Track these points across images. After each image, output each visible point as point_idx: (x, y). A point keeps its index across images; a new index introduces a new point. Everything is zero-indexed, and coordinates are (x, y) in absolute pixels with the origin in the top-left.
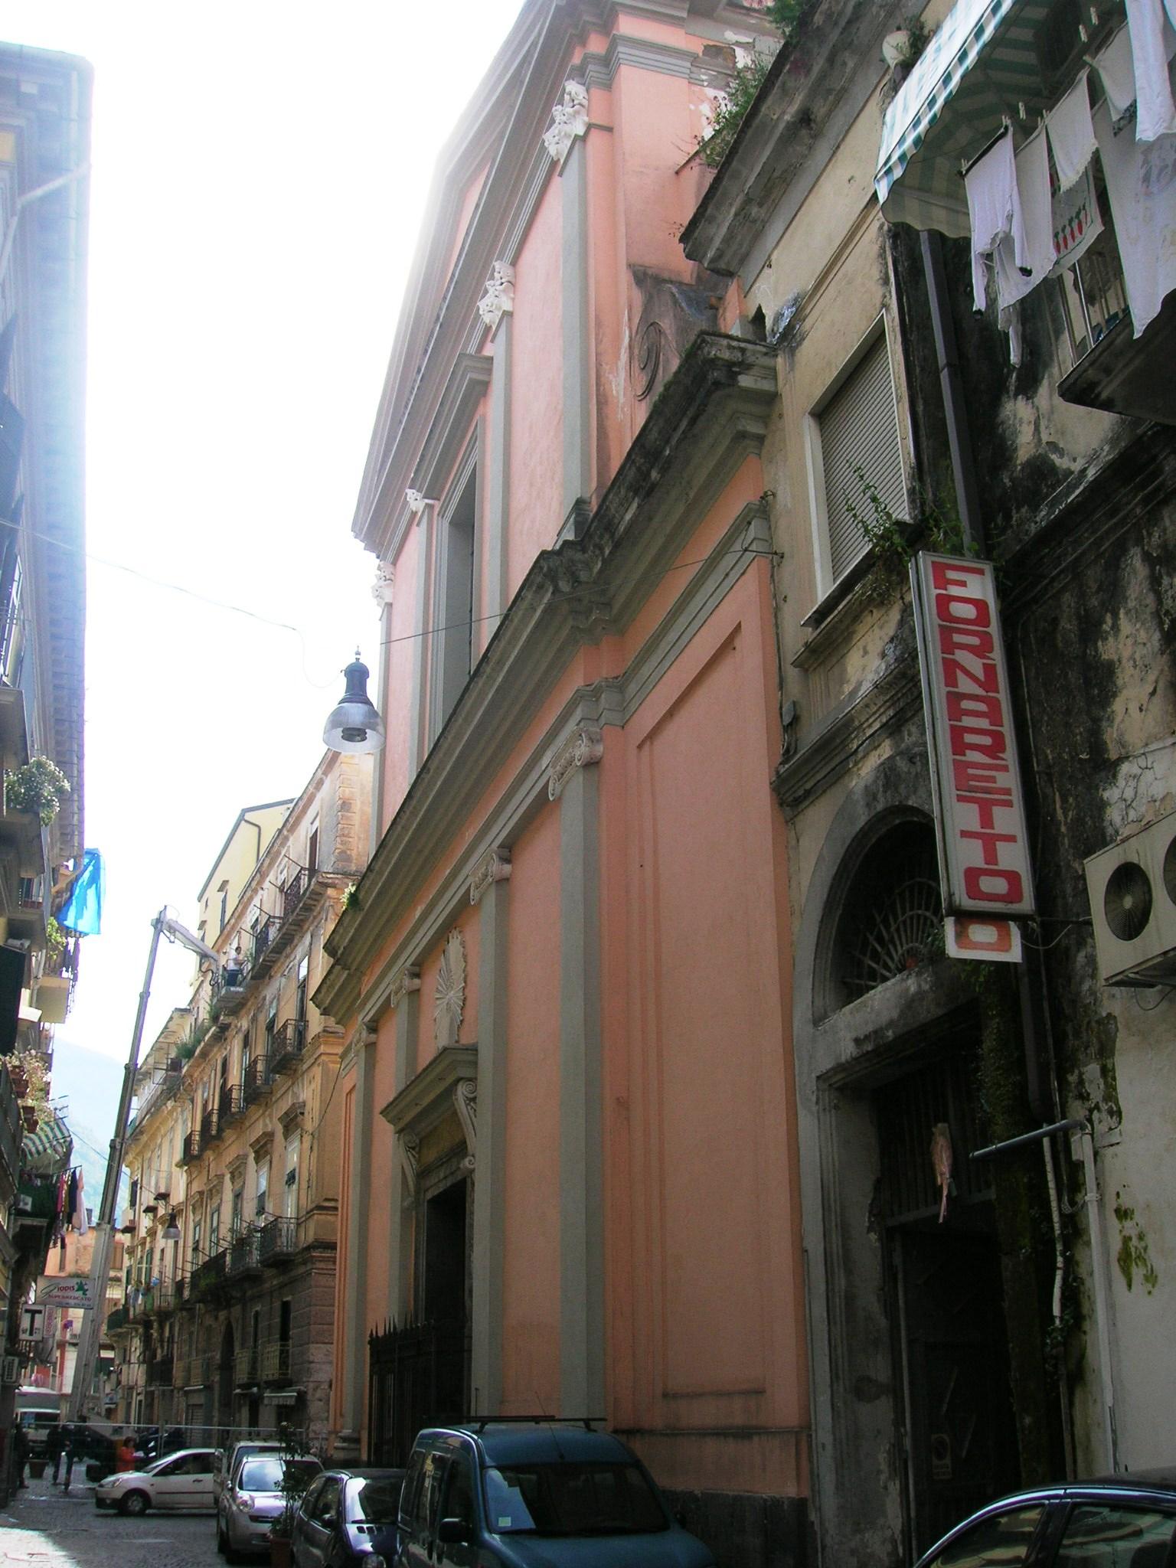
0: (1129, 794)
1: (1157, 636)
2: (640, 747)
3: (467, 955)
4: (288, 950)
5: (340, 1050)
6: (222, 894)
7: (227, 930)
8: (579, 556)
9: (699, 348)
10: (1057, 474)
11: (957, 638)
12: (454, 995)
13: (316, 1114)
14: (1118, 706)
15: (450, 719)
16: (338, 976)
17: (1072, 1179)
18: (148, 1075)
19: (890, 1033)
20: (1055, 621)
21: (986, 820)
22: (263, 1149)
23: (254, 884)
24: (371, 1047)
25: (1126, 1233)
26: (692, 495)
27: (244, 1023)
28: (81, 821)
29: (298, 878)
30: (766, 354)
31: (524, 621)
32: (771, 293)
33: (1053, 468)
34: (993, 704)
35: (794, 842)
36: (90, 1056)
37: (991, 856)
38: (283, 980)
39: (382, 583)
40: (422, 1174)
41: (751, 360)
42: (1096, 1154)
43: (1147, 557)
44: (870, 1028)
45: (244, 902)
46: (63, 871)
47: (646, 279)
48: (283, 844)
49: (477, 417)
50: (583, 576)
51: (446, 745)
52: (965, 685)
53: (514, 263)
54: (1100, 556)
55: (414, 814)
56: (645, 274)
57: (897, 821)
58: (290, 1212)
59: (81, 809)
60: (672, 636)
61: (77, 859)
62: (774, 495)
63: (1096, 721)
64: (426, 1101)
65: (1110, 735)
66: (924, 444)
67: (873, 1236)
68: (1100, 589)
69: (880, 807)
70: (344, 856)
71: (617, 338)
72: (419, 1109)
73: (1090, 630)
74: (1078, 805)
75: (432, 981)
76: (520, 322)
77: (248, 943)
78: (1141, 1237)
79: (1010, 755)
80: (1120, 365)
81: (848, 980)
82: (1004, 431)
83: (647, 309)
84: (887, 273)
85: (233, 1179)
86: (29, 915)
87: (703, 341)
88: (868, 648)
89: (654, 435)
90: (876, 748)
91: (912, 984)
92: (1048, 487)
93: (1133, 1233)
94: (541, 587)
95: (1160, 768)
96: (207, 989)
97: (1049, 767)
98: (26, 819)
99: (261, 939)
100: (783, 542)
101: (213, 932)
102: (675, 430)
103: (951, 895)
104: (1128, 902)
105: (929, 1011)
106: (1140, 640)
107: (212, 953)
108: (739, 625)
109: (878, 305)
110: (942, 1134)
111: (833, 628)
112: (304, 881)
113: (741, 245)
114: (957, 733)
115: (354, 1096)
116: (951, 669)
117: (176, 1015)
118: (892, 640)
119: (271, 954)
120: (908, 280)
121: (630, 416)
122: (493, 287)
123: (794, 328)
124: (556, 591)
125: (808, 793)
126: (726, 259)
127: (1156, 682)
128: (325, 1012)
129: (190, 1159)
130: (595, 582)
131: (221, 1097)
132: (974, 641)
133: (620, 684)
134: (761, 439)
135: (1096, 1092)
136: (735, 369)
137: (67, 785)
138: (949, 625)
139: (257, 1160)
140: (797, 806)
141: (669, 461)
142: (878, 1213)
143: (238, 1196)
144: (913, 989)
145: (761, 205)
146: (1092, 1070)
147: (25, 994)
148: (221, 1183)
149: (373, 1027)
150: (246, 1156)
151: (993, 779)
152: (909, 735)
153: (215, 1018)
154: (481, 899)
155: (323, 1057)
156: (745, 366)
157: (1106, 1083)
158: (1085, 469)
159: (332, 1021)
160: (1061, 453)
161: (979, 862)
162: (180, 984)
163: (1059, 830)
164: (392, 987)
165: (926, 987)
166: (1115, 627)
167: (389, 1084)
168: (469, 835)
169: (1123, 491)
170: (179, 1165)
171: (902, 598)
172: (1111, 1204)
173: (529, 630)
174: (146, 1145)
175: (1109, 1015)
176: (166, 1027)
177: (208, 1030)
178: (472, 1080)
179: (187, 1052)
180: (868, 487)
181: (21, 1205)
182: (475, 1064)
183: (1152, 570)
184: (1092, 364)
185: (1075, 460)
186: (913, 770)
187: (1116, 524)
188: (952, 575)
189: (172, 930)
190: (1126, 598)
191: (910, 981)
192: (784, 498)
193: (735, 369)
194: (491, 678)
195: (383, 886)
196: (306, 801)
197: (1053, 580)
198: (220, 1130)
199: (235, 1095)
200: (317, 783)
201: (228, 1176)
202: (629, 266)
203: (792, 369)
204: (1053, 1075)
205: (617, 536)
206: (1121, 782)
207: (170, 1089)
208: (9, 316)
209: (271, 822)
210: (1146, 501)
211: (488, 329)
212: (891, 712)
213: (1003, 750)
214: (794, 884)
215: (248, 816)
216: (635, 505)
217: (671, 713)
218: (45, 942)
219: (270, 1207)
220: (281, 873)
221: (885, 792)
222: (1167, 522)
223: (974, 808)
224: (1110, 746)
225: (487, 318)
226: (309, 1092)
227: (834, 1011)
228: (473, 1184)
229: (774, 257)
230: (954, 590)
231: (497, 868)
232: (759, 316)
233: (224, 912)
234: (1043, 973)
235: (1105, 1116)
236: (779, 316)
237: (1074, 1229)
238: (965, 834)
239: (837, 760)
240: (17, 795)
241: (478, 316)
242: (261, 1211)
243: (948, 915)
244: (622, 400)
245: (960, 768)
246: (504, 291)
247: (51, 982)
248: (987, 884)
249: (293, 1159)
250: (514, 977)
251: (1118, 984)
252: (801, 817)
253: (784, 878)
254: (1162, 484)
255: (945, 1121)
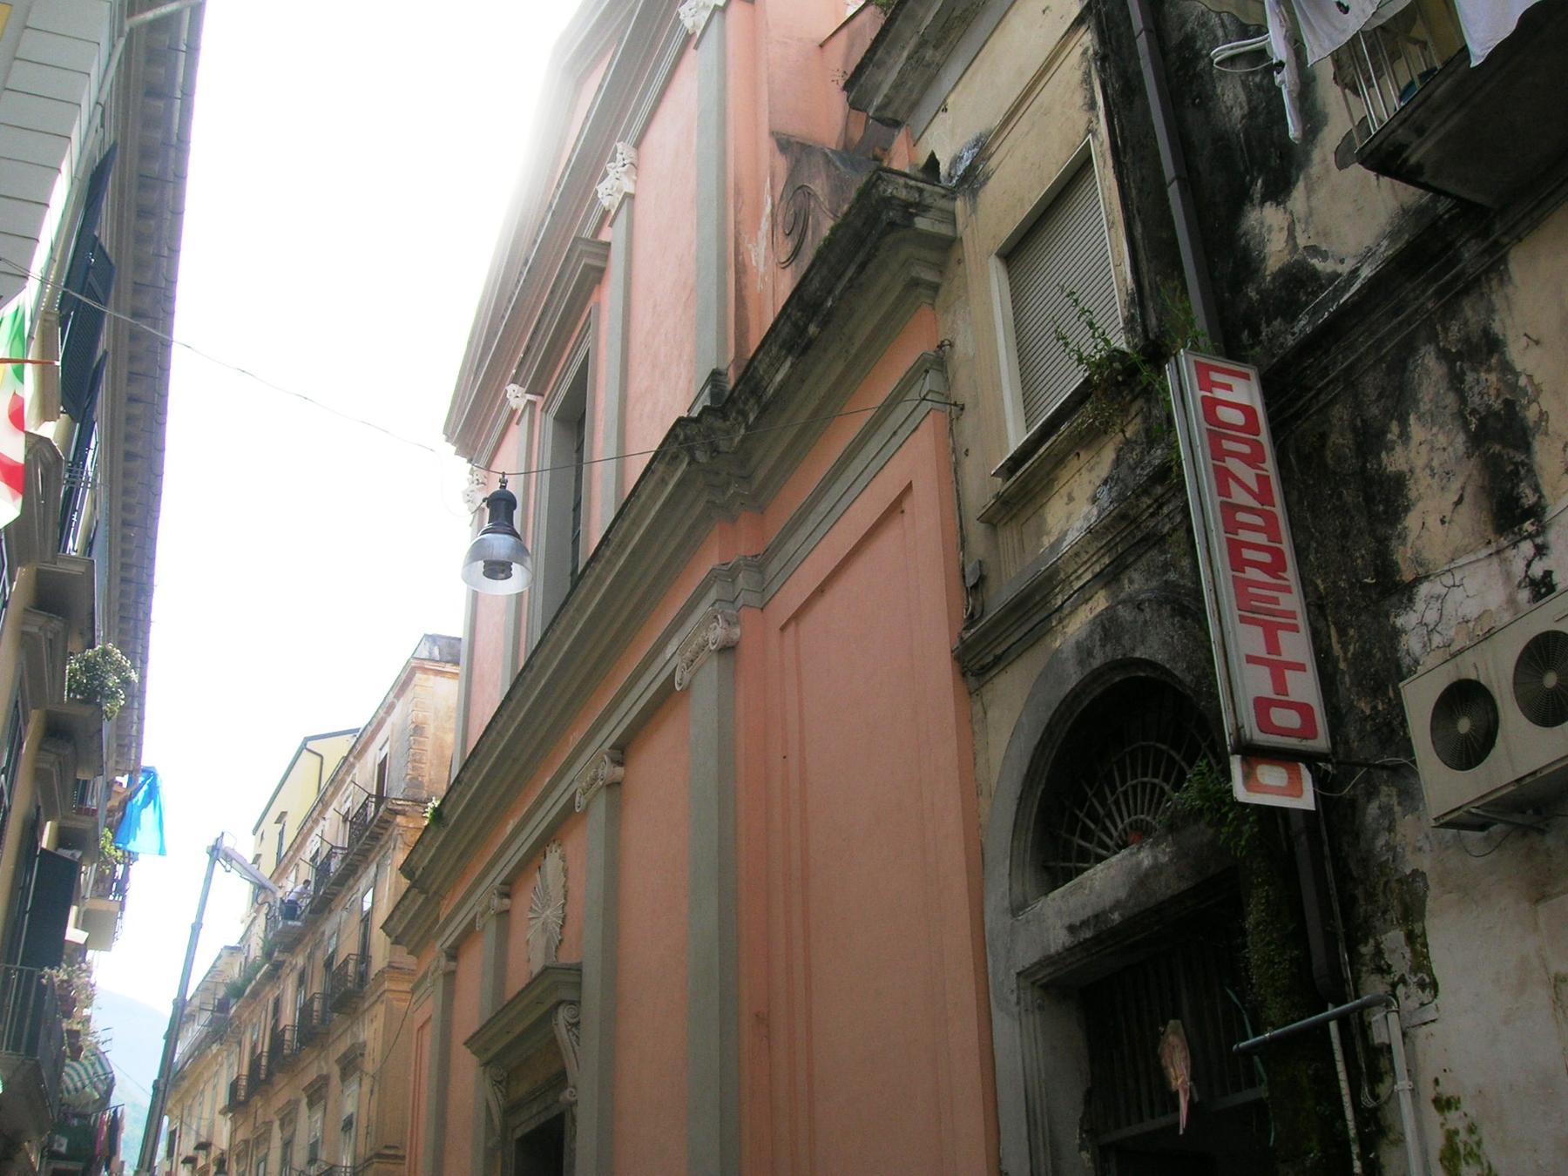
0: (1431, 617)
1: (1461, 438)
2: (783, 629)
3: (568, 871)
4: (351, 882)
5: (407, 987)
6: (280, 827)
7: (283, 864)
8: (718, 424)
9: (874, 185)
10: (1319, 279)
11: (1228, 445)
12: (551, 914)
13: (378, 1056)
14: (1412, 521)
15: (551, 624)
16: (414, 901)
17: (1372, 1064)
18: (192, 1017)
19: (1116, 916)
20: (1323, 436)
21: (1273, 645)
22: (317, 1093)
23: (315, 815)
24: (450, 976)
25: (1450, 1126)
26: (853, 351)
27: (300, 961)
28: (140, 731)
29: (365, 806)
30: (944, 196)
31: (653, 498)
32: (945, 138)
33: (1314, 274)
34: (1270, 518)
35: (981, 714)
36: (148, 969)
37: (1280, 685)
38: (345, 914)
39: (475, 487)
40: (511, 1110)
41: (929, 201)
42: (1404, 1035)
43: (1443, 354)
44: (1089, 912)
45: (304, 833)
46: (116, 788)
47: (791, 147)
48: (348, 772)
49: (591, 304)
50: (723, 445)
51: (553, 639)
52: (1240, 497)
53: (637, 145)
54: (1380, 360)
55: (512, 718)
56: (789, 142)
57: (1117, 679)
58: (346, 1161)
59: (141, 719)
60: (824, 507)
61: (133, 774)
62: (951, 345)
63: (1383, 541)
64: (518, 1029)
65: (1402, 556)
66: (1144, 266)
67: (1085, 1155)
68: (1380, 396)
69: (1097, 662)
70: (415, 783)
71: (758, 206)
72: (510, 1037)
73: (1370, 440)
74: (1361, 636)
75: (523, 901)
76: (641, 206)
77: (306, 872)
78: (1472, 1130)
79: (1291, 574)
80: (1435, 125)
81: (1052, 864)
82: (1248, 243)
83: (793, 173)
84: (1093, 99)
85: (282, 1126)
86: (83, 823)
87: (879, 178)
88: (1075, 494)
89: (816, 283)
90: (1087, 601)
91: (1145, 858)
92: (1307, 294)
93: (1461, 1126)
94: (675, 457)
95: (1472, 585)
96: (262, 921)
97: (1320, 598)
98: (87, 711)
99: (322, 870)
100: (963, 393)
101: (267, 868)
102: (839, 278)
103: (1238, 729)
104: (1464, 725)
105: (1168, 886)
106: (1437, 445)
107: (269, 884)
108: (909, 487)
109: (1082, 133)
110: (1175, 1033)
111: (1031, 474)
112: (372, 809)
113: (911, 91)
114: (1235, 547)
115: (428, 1028)
116: (1223, 477)
117: (225, 953)
118: (1105, 482)
119: (334, 882)
120: (1122, 98)
121: (773, 286)
122: (614, 169)
123: (976, 168)
124: (693, 460)
125: (998, 659)
126: (896, 104)
127: (1463, 488)
128: (397, 941)
129: (237, 1105)
130: (734, 453)
131: (272, 1039)
132: (1246, 449)
133: (759, 563)
134: (935, 288)
135: (1400, 960)
136: (911, 209)
137: (134, 676)
138: (1217, 433)
139: (311, 1105)
140: (983, 674)
141: (831, 313)
142: (1091, 1130)
143: (287, 1144)
144: (1147, 863)
145: (936, 47)
146: (1393, 939)
147: (74, 910)
148: (269, 1131)
149: (454, 954)
150: (297, 1102)
151: (1275, 601)
152: (1131, 582)
153: (268, 955)
154: (588, 805)
155: (388, 995)
156: (922, 208)
157: (1413, 951)
158: (1357, 269)
159: (402, 950)
160: (1324, 256)
161: (1268, 691)
162: (233, 921)
163: (1336, 667)
164: (478, 909)
165: (1164, 859)
166: (1405, 436)
167: (472, 1011)
168: (576, 737)
169: (1409, 286)
170: (224, 1112)
171: (1123, 431)
172: (1428, 1092)
173: (657, 507)
174: (187, 1091)
175: (1415, 872)
176: (214, 966)
177: (260, 967)
178: (575, 1003)
179: (236, 991)
180: (1083, 312)
181: (55, 1147)
182: (579, 986)
183: (1451, 368)
184: (1400, 125)
185: (1342, 261)
186: (1140, 619)
187: (1400, 323)
188: (1216, 377)
189: (229, 858)
190: (1416, 402)
191: (1142, 855)
192: (964, 345)
193: (911, 209)
194: (611, 562)
195: (471, 799)
196: (377, 724)
197: (1319, 392)
198: (270, 1074)
199: (287, 1036)
200: (388, 708)
201: (277, 1124)
202: (772, 133)
203: (974, 210)
204: (1341, 947)
205: (764, 399)
206: (1420, 605)
207: (216, 1032)
208: (107, 148)
209: (335, 751)
210: (1439, 294)
211: (606, 213)
212: (1107, 560)
213: (1285, 570)
214: (981, 761)
215: (310, 745)
216: (788, 364)
217: (821, 590)
218: (98, 855)
219: (323, 1155)
220: (348, 801)
221: (1103, 646)
222: (1469, 313)
223: (1258, 632)
224: (1403, 566)
225: (606, 202)
226: (370, 1031)
227: (1037, 898)
228: (574, 1120)
229: (949, 101)
230: (1220, 394)
231: (609, 771)
232: (933, 163)
233: (280, 844)
234: (1323, 828)
235: (1413, 989)
236: (957, 159)
237: (1375, 1127)
238: (1251, 659)
239: (1037, 619)
240: (79, 684)
241: (596, 199)
242: (313, 1160)
243: (1235, 752)
244: (762, 269)
245: (1241, 586)
246: (626, 173)
247: (100, 905)
248: (1281, 717)
249: (349, 1107)
250: (637, 883)
251: (1447, 825)
252: (989, 686)
253: (969, 758)
254: (1463, 272)
255: (1175, 1017)
